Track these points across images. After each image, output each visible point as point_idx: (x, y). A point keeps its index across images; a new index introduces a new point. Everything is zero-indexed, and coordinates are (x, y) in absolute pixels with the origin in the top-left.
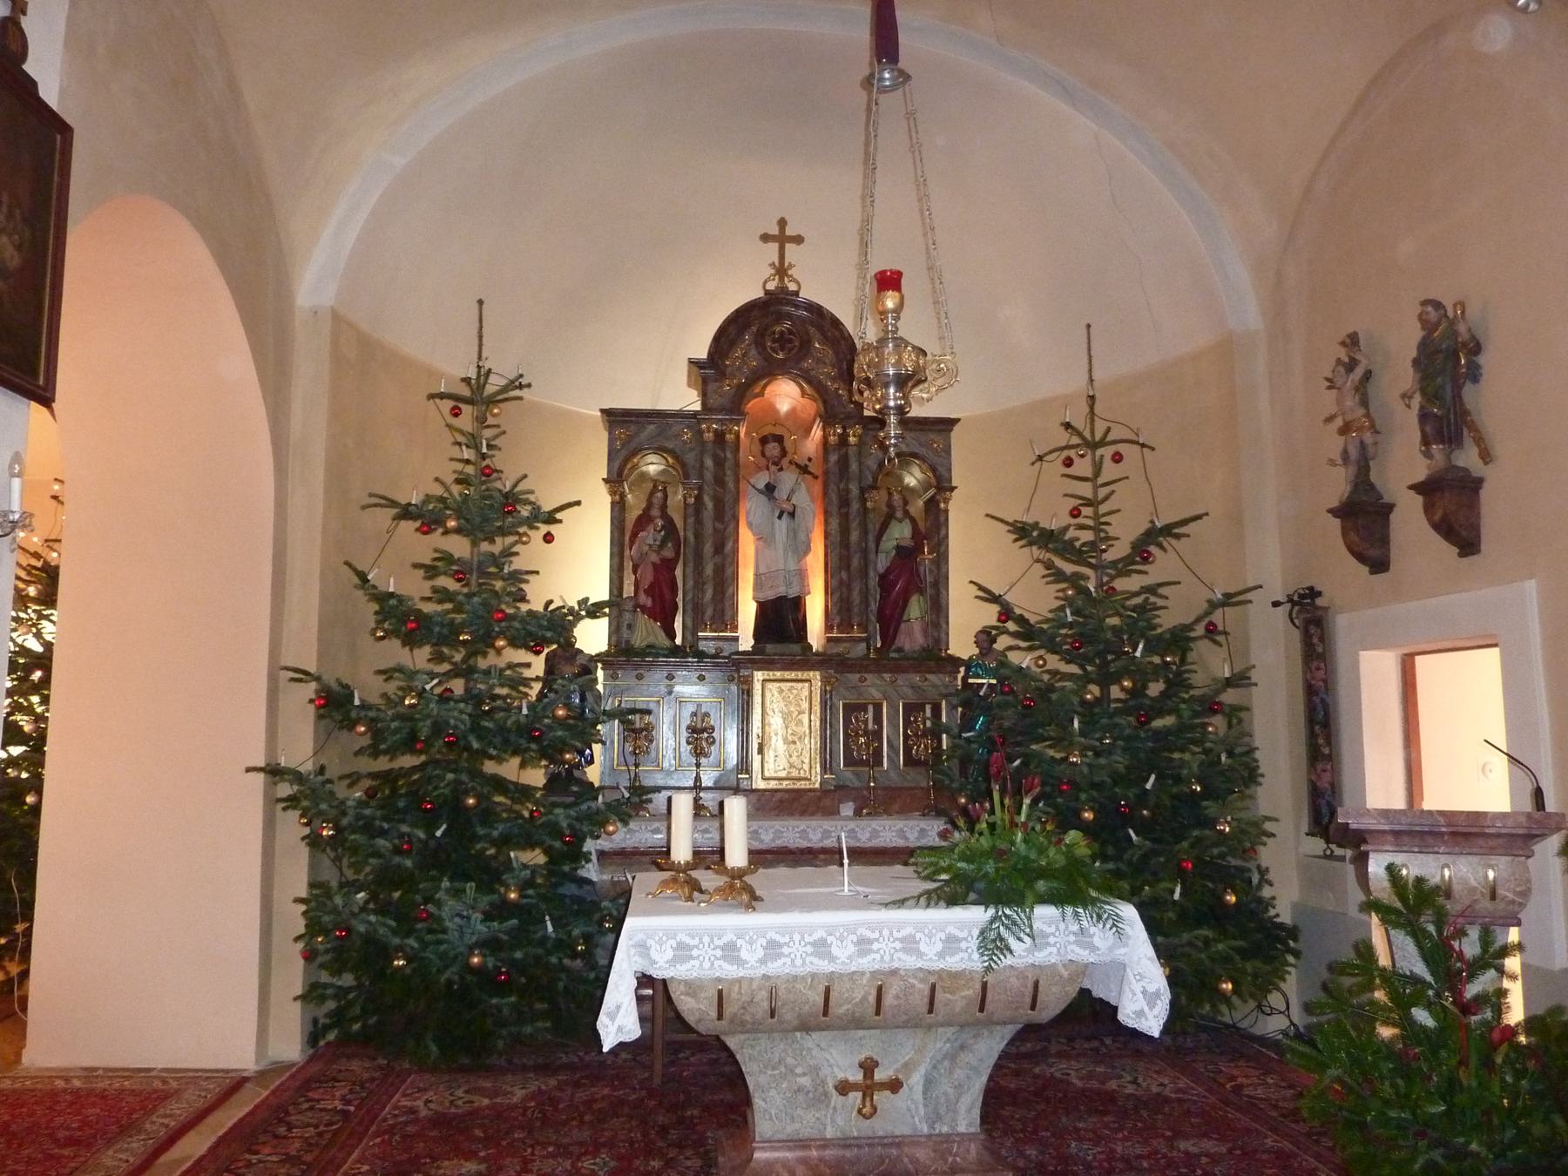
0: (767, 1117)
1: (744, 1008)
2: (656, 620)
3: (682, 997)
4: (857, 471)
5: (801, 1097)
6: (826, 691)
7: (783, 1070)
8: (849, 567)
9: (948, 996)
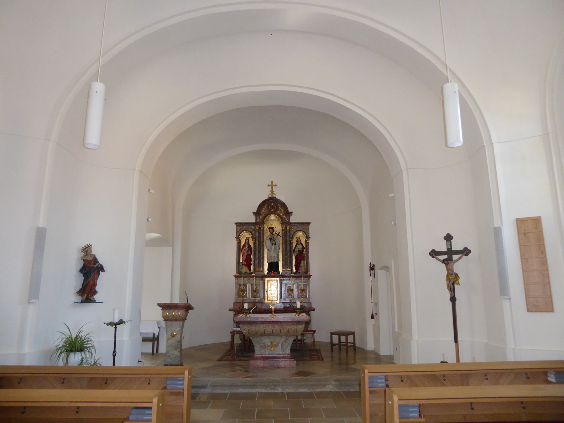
8: (287, 255)
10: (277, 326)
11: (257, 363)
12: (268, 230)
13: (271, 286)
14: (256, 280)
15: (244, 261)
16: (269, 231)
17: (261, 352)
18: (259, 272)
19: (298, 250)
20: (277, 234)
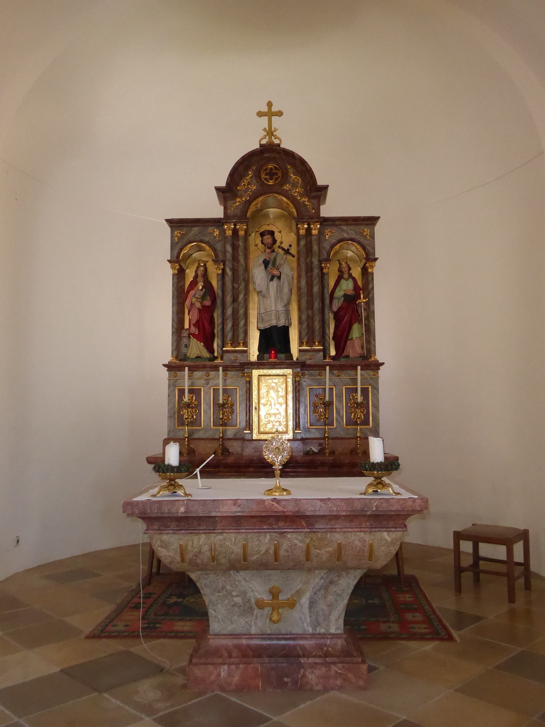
0: (217, 620)
1: (196, 556)
2: (201, 342)
3: (159, 549)
4: (317, 250)
5: (236, 609)
6: (295, 381)
7: (225, 592)
8: (313, 307)
9: (318, 551)
10: (294, 535)
11: (219, 675)
12: (259, 240)
13: (268, 392)
14: (225, 375)
15: (192, 326)
16: (263, 243)
17: (234, 626)
18: (235, 354)
19: (342, 293)
20: (283, 249)
